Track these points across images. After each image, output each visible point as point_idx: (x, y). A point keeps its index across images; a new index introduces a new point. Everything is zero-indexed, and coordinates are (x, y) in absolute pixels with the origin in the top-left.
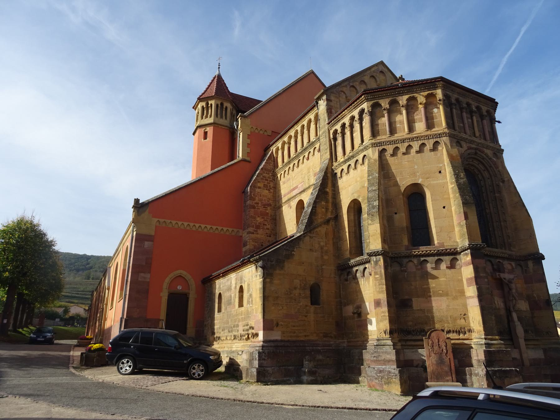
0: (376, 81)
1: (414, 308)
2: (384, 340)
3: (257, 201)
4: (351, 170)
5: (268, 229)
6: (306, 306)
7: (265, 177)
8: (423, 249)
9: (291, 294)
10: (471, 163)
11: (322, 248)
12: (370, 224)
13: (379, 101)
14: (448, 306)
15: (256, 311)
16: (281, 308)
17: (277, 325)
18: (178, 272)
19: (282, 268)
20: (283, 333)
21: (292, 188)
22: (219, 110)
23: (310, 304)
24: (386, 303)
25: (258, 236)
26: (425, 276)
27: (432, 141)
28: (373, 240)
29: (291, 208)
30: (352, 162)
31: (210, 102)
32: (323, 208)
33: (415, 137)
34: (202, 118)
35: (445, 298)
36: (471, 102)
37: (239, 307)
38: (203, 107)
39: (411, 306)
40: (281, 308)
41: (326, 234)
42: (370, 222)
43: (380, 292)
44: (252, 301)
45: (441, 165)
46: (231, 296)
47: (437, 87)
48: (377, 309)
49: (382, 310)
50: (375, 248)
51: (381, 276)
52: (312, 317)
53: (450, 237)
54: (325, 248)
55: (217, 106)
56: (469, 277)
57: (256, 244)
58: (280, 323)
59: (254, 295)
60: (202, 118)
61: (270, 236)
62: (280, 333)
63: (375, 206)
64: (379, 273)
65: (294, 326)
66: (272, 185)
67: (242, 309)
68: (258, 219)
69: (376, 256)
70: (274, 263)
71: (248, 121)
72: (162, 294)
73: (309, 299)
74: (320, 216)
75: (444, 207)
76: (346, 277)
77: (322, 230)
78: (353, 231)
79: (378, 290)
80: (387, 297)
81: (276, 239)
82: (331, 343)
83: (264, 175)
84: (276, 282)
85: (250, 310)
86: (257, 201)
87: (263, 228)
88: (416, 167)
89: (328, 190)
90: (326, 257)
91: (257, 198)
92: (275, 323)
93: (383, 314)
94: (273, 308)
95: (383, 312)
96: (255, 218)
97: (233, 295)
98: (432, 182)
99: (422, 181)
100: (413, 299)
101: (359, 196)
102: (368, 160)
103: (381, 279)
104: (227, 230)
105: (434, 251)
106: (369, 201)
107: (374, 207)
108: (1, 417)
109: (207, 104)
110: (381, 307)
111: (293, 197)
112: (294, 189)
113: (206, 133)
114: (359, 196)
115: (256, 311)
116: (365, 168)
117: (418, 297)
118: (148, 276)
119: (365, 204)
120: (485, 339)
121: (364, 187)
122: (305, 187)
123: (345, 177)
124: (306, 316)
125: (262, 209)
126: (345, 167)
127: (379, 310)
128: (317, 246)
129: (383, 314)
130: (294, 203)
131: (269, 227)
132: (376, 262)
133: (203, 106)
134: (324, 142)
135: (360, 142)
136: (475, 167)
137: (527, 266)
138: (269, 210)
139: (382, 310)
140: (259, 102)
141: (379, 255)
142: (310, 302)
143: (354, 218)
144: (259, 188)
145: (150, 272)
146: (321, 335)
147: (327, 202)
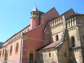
4: (71, 30)
8: (73, 48)
15: (56, 58)
18: (31, 49)
25: (47, 42)
28: (78, 43)
30: (72, 29)
37: (49, 57)
44: (54, 56)
46: (46, 55)
52: (65, 59)
66: (49, 31)
71: (43, 17)
77: (66, 42)
84: (60, 52)
85: (53, 58)
104: (40, 40)
112: (55, 32)
115: (56, 58)
118: (26, 49)
122: (58, 32)
126: (70, 29)
127: (81, 58)
130: (55, 35)
134: (64, 23)
135: (71, 26)
138: (49, 36)
140: (44, 13)
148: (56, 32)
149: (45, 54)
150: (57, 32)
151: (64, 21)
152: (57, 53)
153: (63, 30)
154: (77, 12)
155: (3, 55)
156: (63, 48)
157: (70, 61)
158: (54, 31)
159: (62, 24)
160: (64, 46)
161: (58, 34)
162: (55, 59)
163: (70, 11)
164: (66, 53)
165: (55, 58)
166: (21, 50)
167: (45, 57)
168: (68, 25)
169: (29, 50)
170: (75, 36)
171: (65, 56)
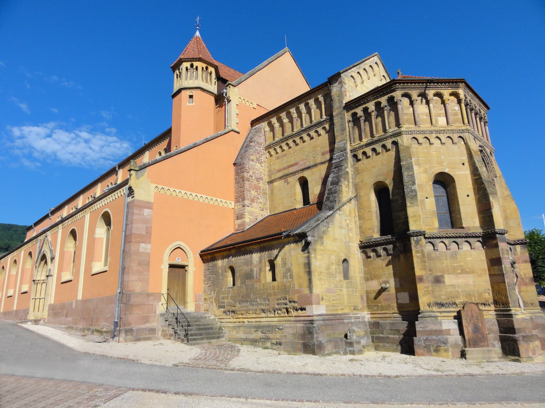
0: (373, 71)
1: (446, 284)
2: (427, 312)
3: (251, 173)
5: (261, 203)
7: (257, 150)
11: (348, 226)
14: (474, 282)
16: (323, 283)
17: (322, 299)
20: (327, 306)
21: (290, 164)
23: (343, 279)
25: (253, 209)
29: (288, 183)
34: (186, 79)
35: (472, 275)
36: (477, 105)
39: (444, 282)
40: (323, 283)
41: (350, 212)
44: (291, 276)
46: (252, 270)
52: (345, 290)
54: (350, 226)
57: (252, 217)
58: (324, 297)
60: (186, 79)
61: (263, 210)
62: (324, 307)
64: (420, 251)
65: (334, 300)
67: (275, 283)
68: (252, 192)
69: (417, 236)
70: (316, 238)
73: (342, 274)
82: (359, 315)
83: (257, 148)
84: (319, 257)
86: (251, 173)
87: (257, 202)
88: (443, 157)
89: (347, 170)
90: (351, 235)
91: (251, 172)
92: (321, 297)
93: (426, 289)
96: (250, 191)
97: (255, 269)
100: (445, 276)
109: (192, 66)
114: (386, 179)
117: (449, 274)
118: (149, 246)
120: (495, 311)
122: (307, 165)
124: (341, 291)
125: (255, 182)
128: (344, 224)
129: (426, 289)
131: (261, 200)
137: (515, 250)
144: (253, 161)
145: (150, 243)
146: (352, 308)
147: (348, 182)
148: (296, 164)
149: (246, 268)
150: (303, 167)
154: (323, 154)
155: (386, 313)
156: (335, 240)
157: (2, 248)
160: (341, 227)
161: (306, 174)
162: (298, 292)
163: (371, 106)
164: (268, 182)
166: (47, 217)
167: (248, 282)
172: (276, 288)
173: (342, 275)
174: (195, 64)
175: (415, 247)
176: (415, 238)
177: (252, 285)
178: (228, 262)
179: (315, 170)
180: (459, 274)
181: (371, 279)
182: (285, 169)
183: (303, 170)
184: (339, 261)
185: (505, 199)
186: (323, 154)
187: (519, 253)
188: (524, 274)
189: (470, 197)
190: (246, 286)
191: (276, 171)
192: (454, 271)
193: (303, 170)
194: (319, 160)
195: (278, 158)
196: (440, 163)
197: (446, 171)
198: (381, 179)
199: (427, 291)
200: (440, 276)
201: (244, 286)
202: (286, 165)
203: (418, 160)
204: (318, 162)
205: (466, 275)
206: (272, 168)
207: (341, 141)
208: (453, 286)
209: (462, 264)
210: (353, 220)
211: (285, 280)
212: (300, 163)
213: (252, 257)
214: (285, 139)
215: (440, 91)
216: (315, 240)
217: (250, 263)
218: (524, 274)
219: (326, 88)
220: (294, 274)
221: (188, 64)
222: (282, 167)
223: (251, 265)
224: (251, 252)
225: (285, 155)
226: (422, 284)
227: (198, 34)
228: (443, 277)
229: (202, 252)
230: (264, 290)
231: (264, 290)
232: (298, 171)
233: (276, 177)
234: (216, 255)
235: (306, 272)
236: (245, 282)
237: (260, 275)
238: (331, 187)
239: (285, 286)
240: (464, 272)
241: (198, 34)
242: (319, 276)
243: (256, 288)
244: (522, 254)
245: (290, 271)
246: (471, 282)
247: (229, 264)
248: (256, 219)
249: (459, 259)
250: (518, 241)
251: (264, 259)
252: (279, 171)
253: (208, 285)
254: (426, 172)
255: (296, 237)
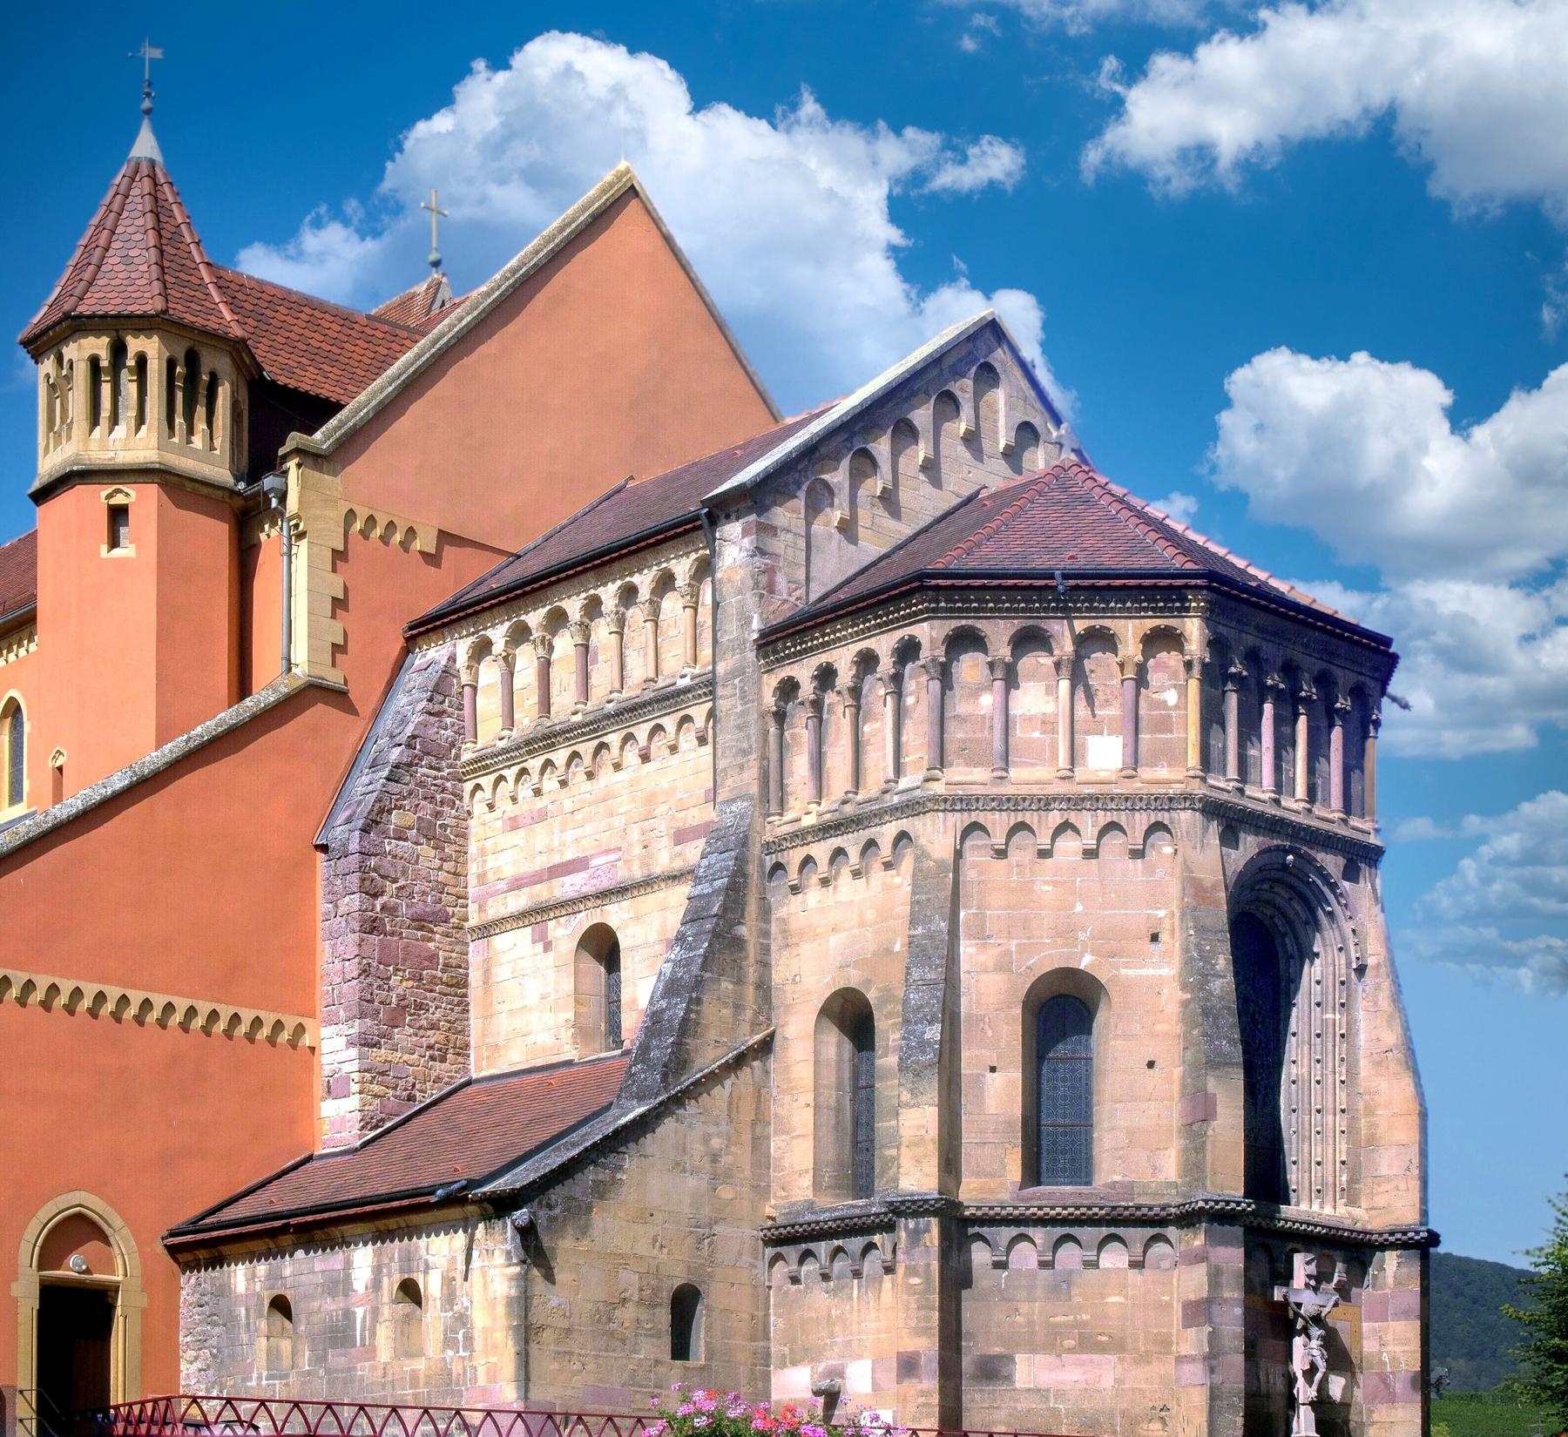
1: (1018, 1385)
6: (657, 1362)
9: (610, 1320)
10: (1265, 896)
11: (715, 1158)
12: (907, 1105)
13: (979, 624)
16: (578, 1366)
19: (584, 1230)
21: (557, 859)
22: (179, 395)
23: (667, 1356)
24: (935, 1365)
26: (1064, 1286)
27: (1142, 820)
29: (548, 947)
30: (851, 843)
31: (135, 344)
32: (726, 1005)
33: (1090, 797)
35: (1113, 1358)
38: (94, 361)
39: (1009, 1378)
40: (578, 1366)
42: (906, 1096)
43: (919, 1332)
44: (469, 1339)
45: (1162, 913)
46: (348, 1315)
47: (1188, 609)
48: (906, 1384)
49: (919, 1387)
50: (914, 1188)
51: (928, 1281)
53: (1155, 1168)
54: (726, 1160)
55: (171, 364)
56: (1192, 1297)
59: (480, 1319)
61: (443, 1060)
63: (929, 1043)
64: (921, 1270)
70: (557, 1211)
72: (143, 1301)
74: (712, 1034)
75: (1151, 1065)
76: (795, 1267)
78: (832, 1102)
79: (913, 1323)
80: (941, 1348)
81: (466, 1070)
85: (457, 1369)
88: (1079, 908)
89: (743, 931)
91: (391, 888)
93: (921, 1400)
94: (555, 1366)
95: (923, 1394)
97: (359, 1312)
98: (1123, 971)
99: (1092, 965)
100: (1018, 1357)
101: (868, 982)
102: (918, 859)
103: (927, 1289)
105: (1101, 1208)
106: (907, 1021)
107: (923, 1045)
108: (1240, 1432)
109: (118, 350)
110: (918, 1377)
111: (562, 905)
113: (118, 514)
116: (902, 879)
117: (1034, 1351)
119: (890, 1015)
121: (889, 952)
122: (622, 875)
123: (813, 896)
128: (698, 1149)
129: (921, 1400)
132: (915, 1236)
133: (94, 361)
136: (1276, 907)
139: (919, 1387)
141: (927, 1213)
142: (669, 1348)
143: (839, 1055)
147: (740, 981)
150: (605, 883)
151: (738, 671)
152: (228, 1214)
153: (693, 852)
154: (680, 837)
158: (506, 842)
159: (699, 712)
161: (615, 915)
165: (482, 1380)
167: (336, 1359)
168: (800, 765)
169: (19, 1238)
170: (886, 998)
171: (680, 1349)
172: (422, 1381)
173: (666, 1342)
174: (135, 344)
175: (907, 1252)
176: (911, 1224)
177: (349, 1369)
178: (269, 1276)
179: (649, 901)
180: (1070, 1350)
181: (794, 1363)
182: (537, 878)
183: (604, 895)
184: (656, 1291)
185: (1379, 1063)
186: (680, 837)
187: (1390, 1281)
188: (1394, 1359)
189: (1156, 1069)
190: (328, 1371)
191: (502, 885)
192: (1050, 1342)
193: (604, 895)
194: (664, 860)
195: (514, 824)
196: (1067, 932)
197: (1085, 962)
198: (853, 979)
199: (925, 1405)
200: (1001, 1357)
201: (322, 1372)
202: (542, 862)
203: (980, 918)
204: (658, 870)
205: (1096, 1357)
206: (489, 865)
207: (734, 800)
208: (1040, 1392)
209: (1085, 1317)
210: (747, 1137)
211: (450, 1353)
212: (594, 862)
213: (348, 1265)
214: (546, 740)
215: (1106, 623)
216: (552, 1219)
217: (340, 1284)
218: (1394, 1359)
219: (700, 538)
220: (476, 1333)
221: (99, 346)
222: (527, 868)
223: (346, 1295)
224: (345, 1243)
225: (542, 816)
226: (915, 1381)
227: (145, 146)
228: (1009, 1359)
229: (173, 1234)
230: (384, 1386)
231: (384, 1386)
232: (586, 898)
233: (503, 911)
234: (225, 1249)
235: (510, 1328)
236: (324, 1358)
237: (373, 1334)
238: (664, 1004)
239: (450, 1374)
240: (1088, 1344)
241: (145, 146)
242: (558, 1342)
243: (362, 1379)
244: (1398, 1282)
245: (464, 1325)
246: (1108, 1381)
247: (272, 1287)
248: (411, 1098)
249: (1076, 1300)
250: (1392, 1234)
251: (390, 1275)
252: (517, 884)
253: (198, 1365)
254: (1003, 966)
255: (486, 1205)
